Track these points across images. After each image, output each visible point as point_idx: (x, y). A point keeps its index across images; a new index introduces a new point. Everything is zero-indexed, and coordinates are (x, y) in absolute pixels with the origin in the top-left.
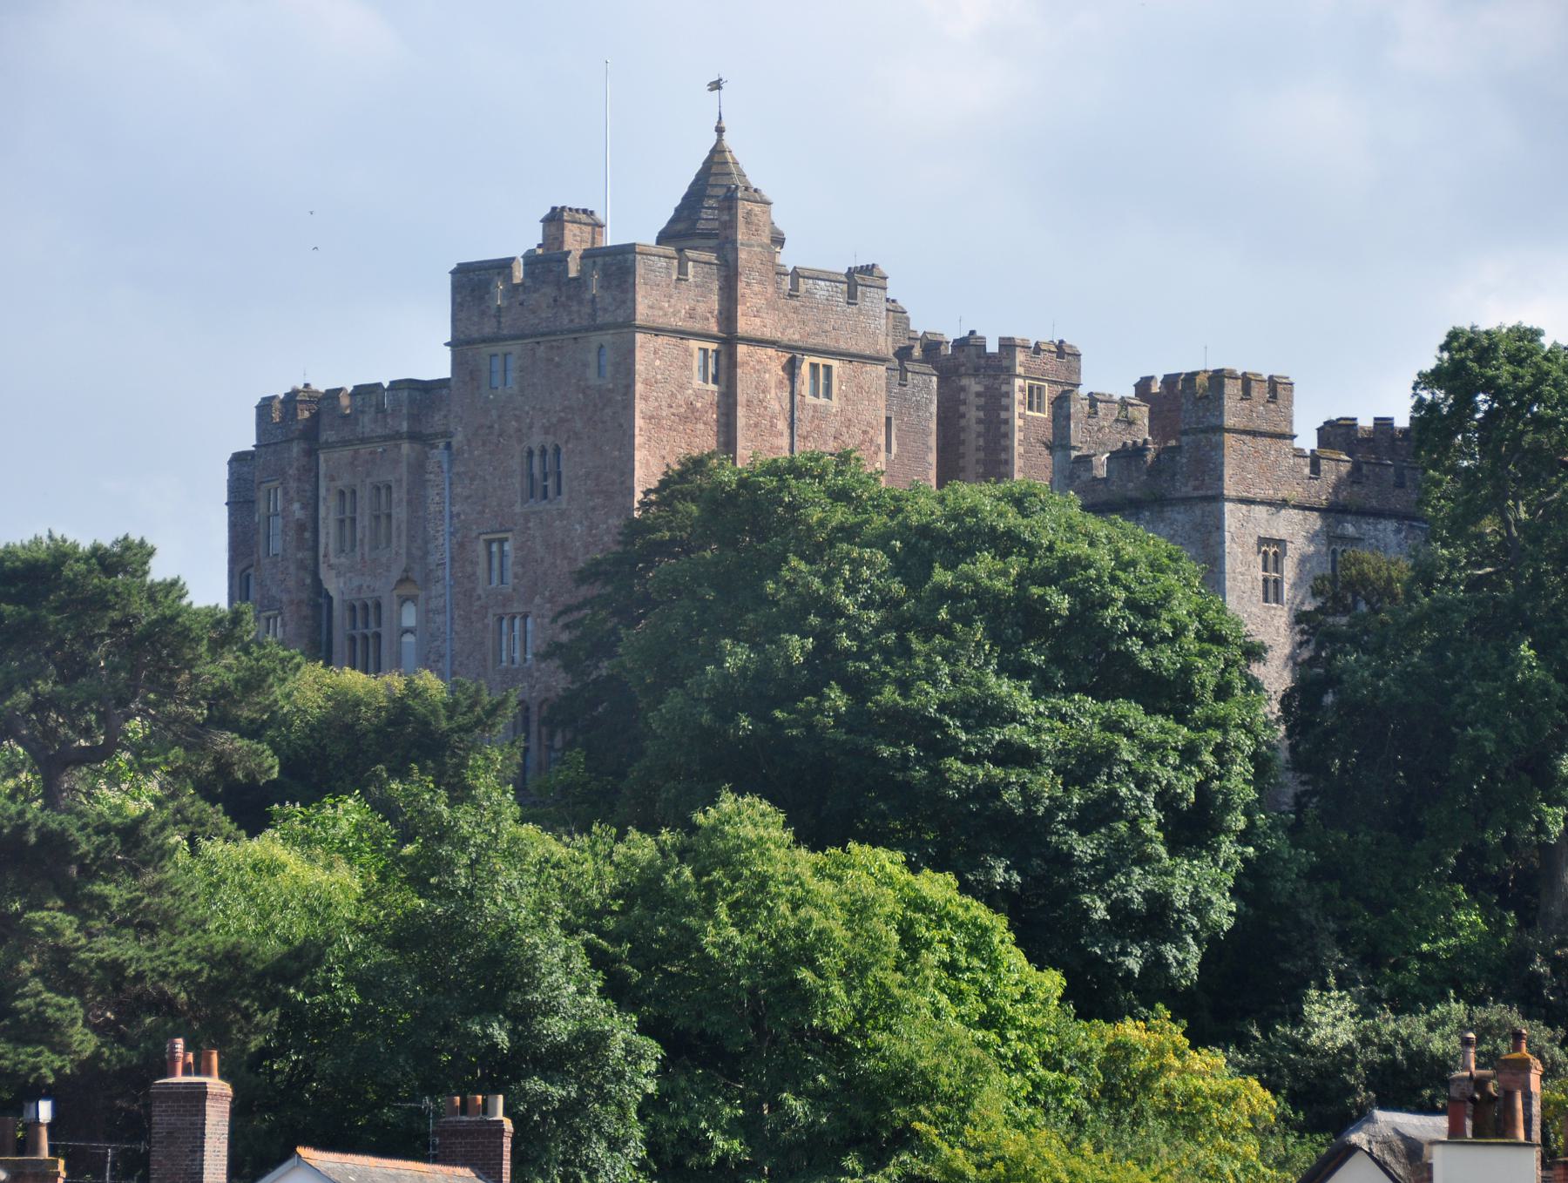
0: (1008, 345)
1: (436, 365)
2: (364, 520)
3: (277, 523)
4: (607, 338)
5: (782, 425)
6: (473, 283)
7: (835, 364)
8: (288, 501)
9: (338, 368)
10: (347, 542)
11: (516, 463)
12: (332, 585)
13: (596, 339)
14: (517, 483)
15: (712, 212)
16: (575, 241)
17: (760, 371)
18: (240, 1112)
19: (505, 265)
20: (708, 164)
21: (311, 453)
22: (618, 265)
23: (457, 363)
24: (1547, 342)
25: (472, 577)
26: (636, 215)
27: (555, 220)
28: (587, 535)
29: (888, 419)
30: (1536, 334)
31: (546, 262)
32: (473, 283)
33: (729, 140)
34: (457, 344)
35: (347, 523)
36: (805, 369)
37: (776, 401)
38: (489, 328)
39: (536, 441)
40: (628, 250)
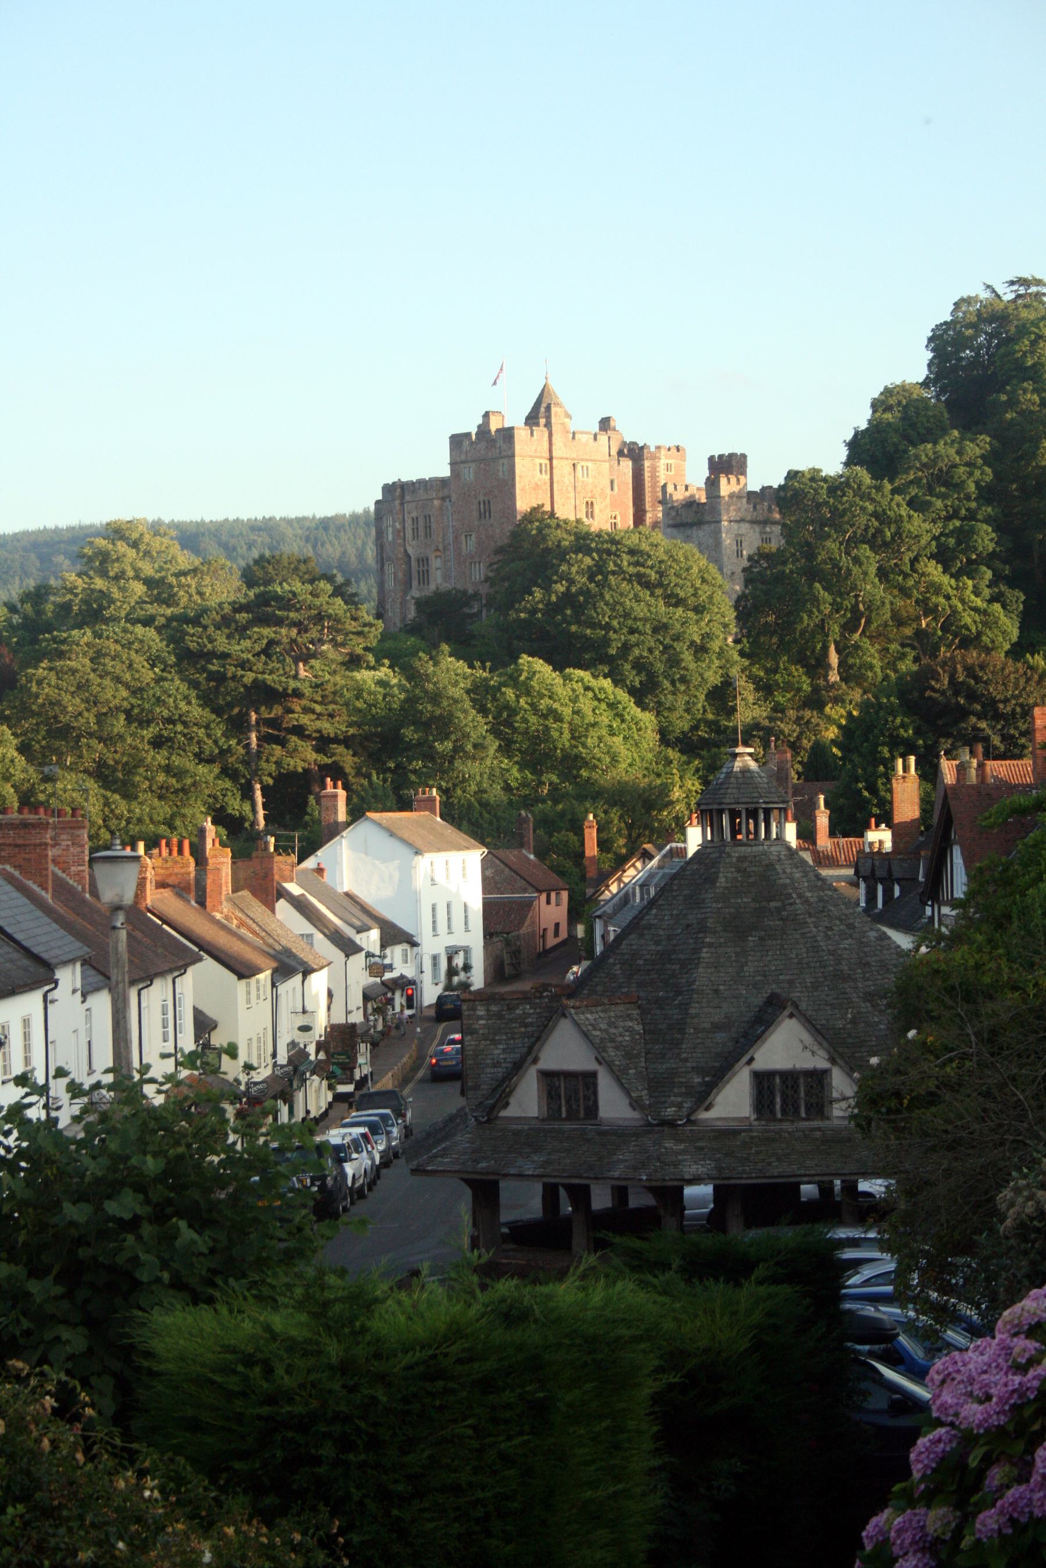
0: (658, 448)
1: (445, 472)
2: (421, 530)
3: (390, 530)
4: (505, 461)
5: (571, 489)
6: (457, 441)
7: (590, 464)
8: (394, 521)
9: (410, 474)
10: (416, 536)
11: (474, 507)
12: (410, 551)
13: (501, 461)
14: (475, 514)
15: (540, 413)
16: (494, 425)
17: (562, 469)
18: (349, 800)
19: (469, 434)
20: (543, 391)
21: (402, 504)
22: (507, 434)
23: (452, 471)
24: (823, 474)
25: (460, 548)
26: (514, 416)
27: (486, 415)
28: (501, 534)
29: (612, 482)
30: (819, 471)
31: (483, 429)
32: (457, 441)
33: (550, 382)
34: (453, 464)
35: (415, 530)
36: (579, 468)
37: (568, 480)
38: (463, 457)
39: (481, 498)
40: (511, 429)
